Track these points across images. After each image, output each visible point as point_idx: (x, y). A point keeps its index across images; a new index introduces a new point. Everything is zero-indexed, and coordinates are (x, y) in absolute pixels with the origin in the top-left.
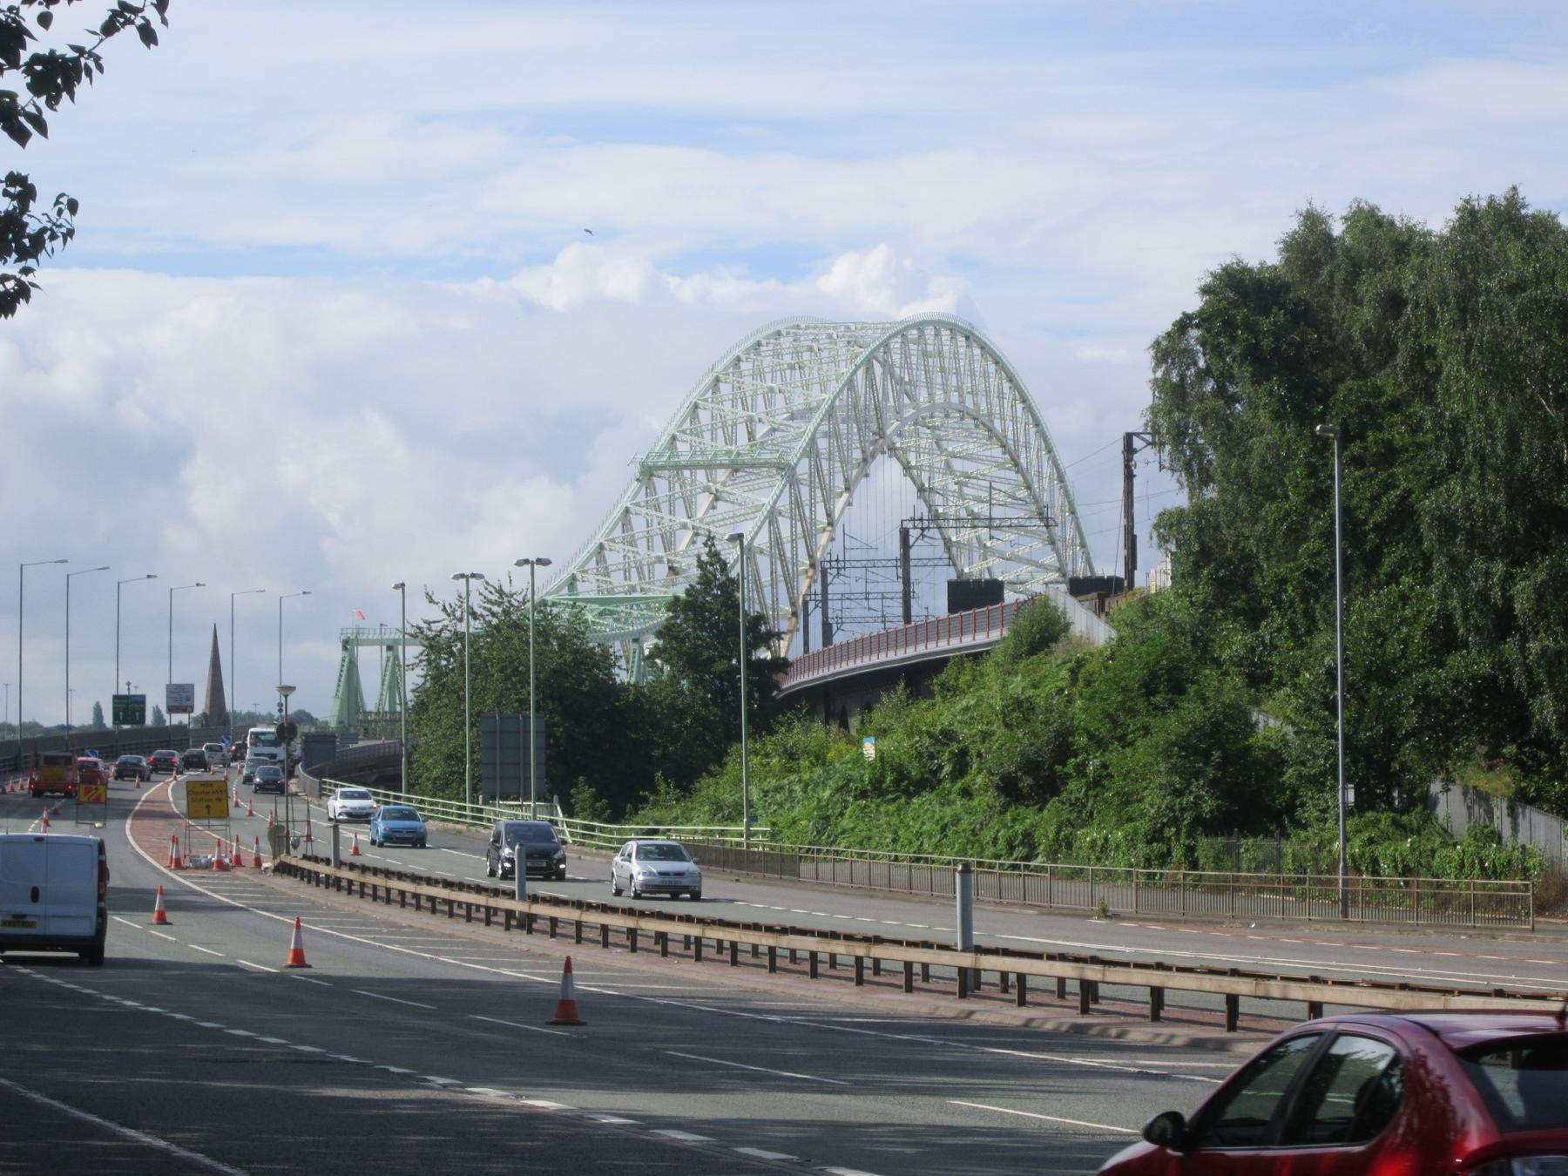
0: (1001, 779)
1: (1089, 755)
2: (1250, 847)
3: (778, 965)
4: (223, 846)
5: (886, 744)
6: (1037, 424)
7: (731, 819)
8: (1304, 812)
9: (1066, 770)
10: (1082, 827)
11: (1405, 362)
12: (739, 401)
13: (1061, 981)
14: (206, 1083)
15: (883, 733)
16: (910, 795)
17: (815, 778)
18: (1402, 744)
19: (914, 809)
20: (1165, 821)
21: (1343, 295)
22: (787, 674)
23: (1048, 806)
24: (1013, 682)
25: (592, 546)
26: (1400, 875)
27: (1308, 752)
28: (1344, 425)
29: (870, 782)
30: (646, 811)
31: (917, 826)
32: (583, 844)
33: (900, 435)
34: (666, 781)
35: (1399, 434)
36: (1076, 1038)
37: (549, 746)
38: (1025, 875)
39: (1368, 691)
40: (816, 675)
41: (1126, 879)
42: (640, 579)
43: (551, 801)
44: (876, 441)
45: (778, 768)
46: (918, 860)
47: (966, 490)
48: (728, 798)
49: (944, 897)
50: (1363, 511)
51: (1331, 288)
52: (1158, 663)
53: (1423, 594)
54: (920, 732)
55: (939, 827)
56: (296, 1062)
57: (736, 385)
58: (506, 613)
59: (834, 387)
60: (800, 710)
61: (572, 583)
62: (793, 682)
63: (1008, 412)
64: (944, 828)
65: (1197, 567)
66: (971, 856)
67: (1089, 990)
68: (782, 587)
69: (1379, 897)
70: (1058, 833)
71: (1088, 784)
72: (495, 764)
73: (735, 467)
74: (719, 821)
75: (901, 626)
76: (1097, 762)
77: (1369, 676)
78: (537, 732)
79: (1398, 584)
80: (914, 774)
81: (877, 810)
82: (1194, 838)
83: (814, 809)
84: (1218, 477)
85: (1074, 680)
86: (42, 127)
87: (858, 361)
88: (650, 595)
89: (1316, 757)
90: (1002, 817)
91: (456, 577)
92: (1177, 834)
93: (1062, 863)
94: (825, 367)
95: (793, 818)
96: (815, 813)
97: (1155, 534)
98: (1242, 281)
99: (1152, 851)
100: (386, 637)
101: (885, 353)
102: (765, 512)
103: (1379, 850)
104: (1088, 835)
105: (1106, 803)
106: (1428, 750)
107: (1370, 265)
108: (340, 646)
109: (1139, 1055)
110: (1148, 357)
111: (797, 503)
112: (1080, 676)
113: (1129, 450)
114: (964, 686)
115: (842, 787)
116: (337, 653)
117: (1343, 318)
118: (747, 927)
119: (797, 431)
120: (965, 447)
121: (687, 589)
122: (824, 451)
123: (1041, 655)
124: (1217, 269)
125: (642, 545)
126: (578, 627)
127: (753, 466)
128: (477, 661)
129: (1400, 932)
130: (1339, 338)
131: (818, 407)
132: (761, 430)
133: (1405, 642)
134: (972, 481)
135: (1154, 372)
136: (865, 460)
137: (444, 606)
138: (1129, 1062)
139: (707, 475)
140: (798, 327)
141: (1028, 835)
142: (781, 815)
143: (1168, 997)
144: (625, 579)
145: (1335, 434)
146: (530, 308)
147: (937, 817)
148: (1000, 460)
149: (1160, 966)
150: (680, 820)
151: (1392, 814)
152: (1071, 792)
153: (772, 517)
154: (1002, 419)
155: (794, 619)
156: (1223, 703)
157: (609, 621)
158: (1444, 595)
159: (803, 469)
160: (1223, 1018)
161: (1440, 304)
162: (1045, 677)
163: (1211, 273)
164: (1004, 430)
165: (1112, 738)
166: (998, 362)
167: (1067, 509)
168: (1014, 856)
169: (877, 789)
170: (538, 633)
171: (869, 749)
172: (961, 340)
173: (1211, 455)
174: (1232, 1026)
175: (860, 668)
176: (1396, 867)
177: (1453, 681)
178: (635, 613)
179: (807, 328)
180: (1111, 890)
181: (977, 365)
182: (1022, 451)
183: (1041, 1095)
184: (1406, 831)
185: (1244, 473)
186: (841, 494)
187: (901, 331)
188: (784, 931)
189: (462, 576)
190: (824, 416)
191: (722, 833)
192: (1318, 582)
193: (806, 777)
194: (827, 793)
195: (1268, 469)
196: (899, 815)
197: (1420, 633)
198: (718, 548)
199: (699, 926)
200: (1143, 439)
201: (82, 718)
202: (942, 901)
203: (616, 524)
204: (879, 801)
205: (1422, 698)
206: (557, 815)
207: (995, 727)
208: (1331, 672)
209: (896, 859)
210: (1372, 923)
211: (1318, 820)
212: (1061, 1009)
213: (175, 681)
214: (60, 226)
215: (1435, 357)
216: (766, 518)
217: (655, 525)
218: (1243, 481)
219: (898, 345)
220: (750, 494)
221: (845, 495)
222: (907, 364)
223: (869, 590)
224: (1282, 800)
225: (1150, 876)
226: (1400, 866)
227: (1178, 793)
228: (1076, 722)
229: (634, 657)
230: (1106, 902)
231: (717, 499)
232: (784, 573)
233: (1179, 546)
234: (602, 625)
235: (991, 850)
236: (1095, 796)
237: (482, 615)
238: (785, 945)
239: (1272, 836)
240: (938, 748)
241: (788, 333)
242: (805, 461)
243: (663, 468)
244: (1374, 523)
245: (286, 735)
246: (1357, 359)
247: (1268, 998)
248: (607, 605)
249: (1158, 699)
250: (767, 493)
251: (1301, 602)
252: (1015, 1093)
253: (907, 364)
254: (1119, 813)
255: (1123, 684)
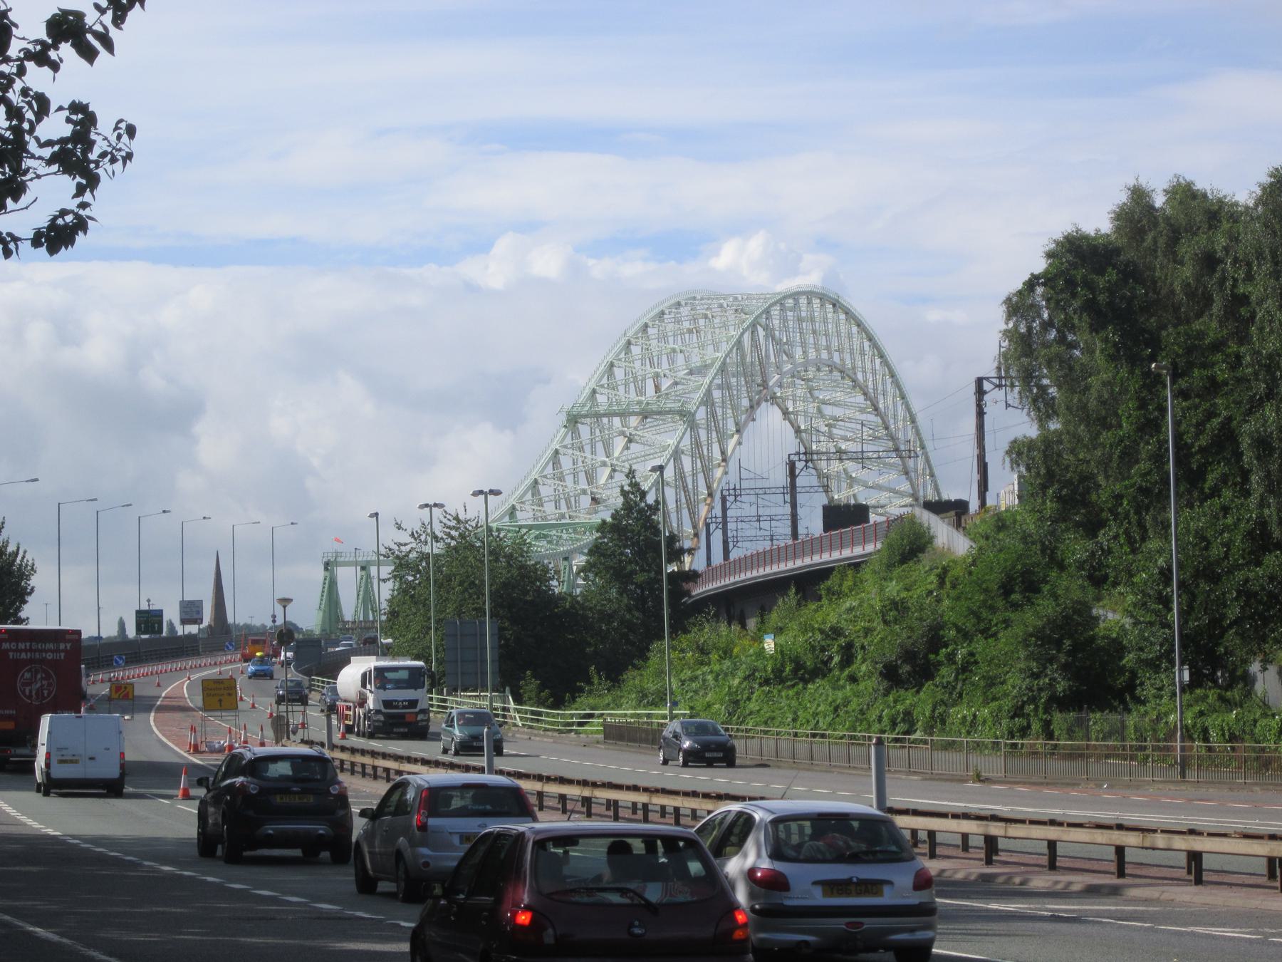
0: (883, 667)
1: (957, 645)
2: (1098, 720)
3: (620, 815)
4: (233, 733)
5: (781, 640)
6: (893, 376)
7: (653, 704)
8: (1143, 690)
9: (938, 658)
10: (953, 706)
11: (1220, 311)
12: (647, 360)
13: (965, 837)
14: (243, 939)
15: (779, 631)
16: (806, 682)
17: (725, 668)
18: (1227, 631)
19: (810, 693)
20: (1025, 699)
21: (1165, 256)
22: (696, 583)
23: (924, 689)
24: (888, 586)
25: (529, 481)
26: (1227, 742)
27: (1146, 639)
28: (1175, 365)
29: (773, 671)
30: (582, 698)
31: (814, 708)
32: (531, 727)
33: (780, 386)
34: (598, 673)
35: (1222, 372)
36: (984, 886)
37: (501, 647)
38: (910, 747)
39: (1197, 586)
40: (719, 584)
41: (993, 748)
42: (568, 508)
43: (504, 692)
44: (761, 391)
45: (692, 661)
46: (814, 736)
47: (835, 431)
48: (651, 687)
49: (840, 767)
50: (1189, 435)
51: (1155, 251)
52: (1014, 567)
53: (1242, 505)
54: (813, 629)
55: (832, 708)
56: (319, 918)
57: (645, 347)
58: (462, 536)
59: (725, 347)
60: (709, 614)
61: (512, 512)
62: (699, 590)
63: (868, 365)
64: (836, 709)
65: (1044, 487)
66: (860, 731)
67: (991, 844)
68: (685, 512)
69: (1211, 760)
70: (933, 711)
71: (957, 670)
72: (457, 661)
73: (645, 415)
74: (644, 706)
75: (790, 542)
76: (964, 651)
77: (1197, 575)
78: (492, 635)
79: (1219, 497)
80: (808, 664)
81: (779, 695)
82: (1050, 714)
83: (726, 695)
84: (1063, 409)
85: (942, 583)
86: (108, 44)
87: (745, 325)
88: (577, 521)
89: (1152, 644)
90: (886, 698)
91: (422, 507)
92: (1036, 709)
93: (938, 736)
94: (717, 331)
95: (707, 703)
96: (727, 698)
97: (1007, 459)
98: (1080, 246)
99: (1015, 725)
100: (360, 559)
101: (767, 318)
102: (670, 451)
103: (1208, 721)
104: (959, 713)
105: (974, 685)
106: (1249, 636)
107: (1186, 231)
108: (323, 567)
109: (1046, 900)
110: (1000, 312)
111: (697, 443)
112: (947, 579)
113: (980, 392)
114: (847, 591)
115: (749, 676)
116: (319, 574)
117: (1167, 275)
118: (686, 794)
119: (696, 384)
120: (833, 395)
121: (612, 514)
122: (717, 400)
123: (911, 563)
124: (1059, 236)
125: (569, 480)
126: (521, 547)
127: (659, 413)
128: (440, 576)
129: (1231, 789)
130: (1163, 292)
131: (713, 364)
132: (665, 384)
133: (1227, 545)
134: (840, 423)
135: (1007, 324)
136: (752, 407)
137: (413, 533)
138: (1039, 906)
139: (621, 421)
140: (694, 298)
141: (908, 713)
142: (696, 700)
143: (1060, 850)
144: (556, 508)
145: (1168, 371)
146: (471, 288)
147: (830, 699)
148: (862, 406)
149: (1053, 823)
150: (612, 706)
151: (1219, 691)
152: (943, 677)
153: (677, 454)
154: (864, 372)
155: (696, 539)
156: (1072, 599)
157: (543, 543)
158: (1262, 504)
159: (701, 414)
160: (1113, 867)
161: (1257, 259)
162: (916, 581)
163: (1055, 241)
164: (865, 381)
165: (976, 631)
166: (859, 324)
167: (918, 445)
168: (897, 731)
169: (778, 677)
170: (491, 553)
171: (769, 644)
172: (829, 307)
173: (1053, 391)
174: (1121, 873)
175: (755, 578)
176: (1223, 735)
177: (1269, 578)
178: (565, 536)
179: (702, 299)
180: (979, 758)
181: (842, 327)
182: (881, 398)
183: (975, 937)
184: (1230, 704)
185: (1084, 407)
186: (733, 435)
187: (781, 299)
188: (657, 791)
189: (427, 505)
190: (718, 371)
191: (649, 716)
192: (1151, 497)
193: (717, 668)
194: (736, 682)
195: (1104, 403)
196: (798, 699)
197: (1240, 537)
198: (638, 480)
199: (645, 794)
200: (991, 383)
201: (109, 631)
202: (838, 770)
203: (547, 464)
204: (780, 687)
205: (1246, 594)
206: (509, 703)
207: (875, 624)
208: (1165, 575)
209: (796, 735)
210: (1206, 783)
211: (1155, 697)
212: (967, 861)
213: (187, 598)
214: (120, 150)
215: (1249, 303)
216: (671, 456)
217: (580, 464)
218: (1081, 413)
219: (777, 312)
220: (658, 436)
221: (736, 437)
222: (785, 328)
223: (760, 513)
224: (1122, 681)
225: (1014, 746)
226: (1227, 734)
227: (1035, 676)
228: (946, 618)
229: (564, 573)
230: (979, 769)
231: (630, 441)
232: (687, 501)
233: (1028, 469)
234: (538, 546)
235: (876, 726)
236: (964, 680)
237: (442, 538)
238: (686, 806)
239: (1116, 711)
240: (828, 642)
241: (686, 304)
242: (703, 409)
243: (586, 416)
244: (1200, 446)
245: (285, 639)
246: (1176, 309)
247: (1154, 849)
248: (542, 529)
249: (1016, 597)
250: (671, 436)
251: (1136, 513)
252: (951, 937)
253: (785, 328)
254: (985, 693)
255: (984, 586)
